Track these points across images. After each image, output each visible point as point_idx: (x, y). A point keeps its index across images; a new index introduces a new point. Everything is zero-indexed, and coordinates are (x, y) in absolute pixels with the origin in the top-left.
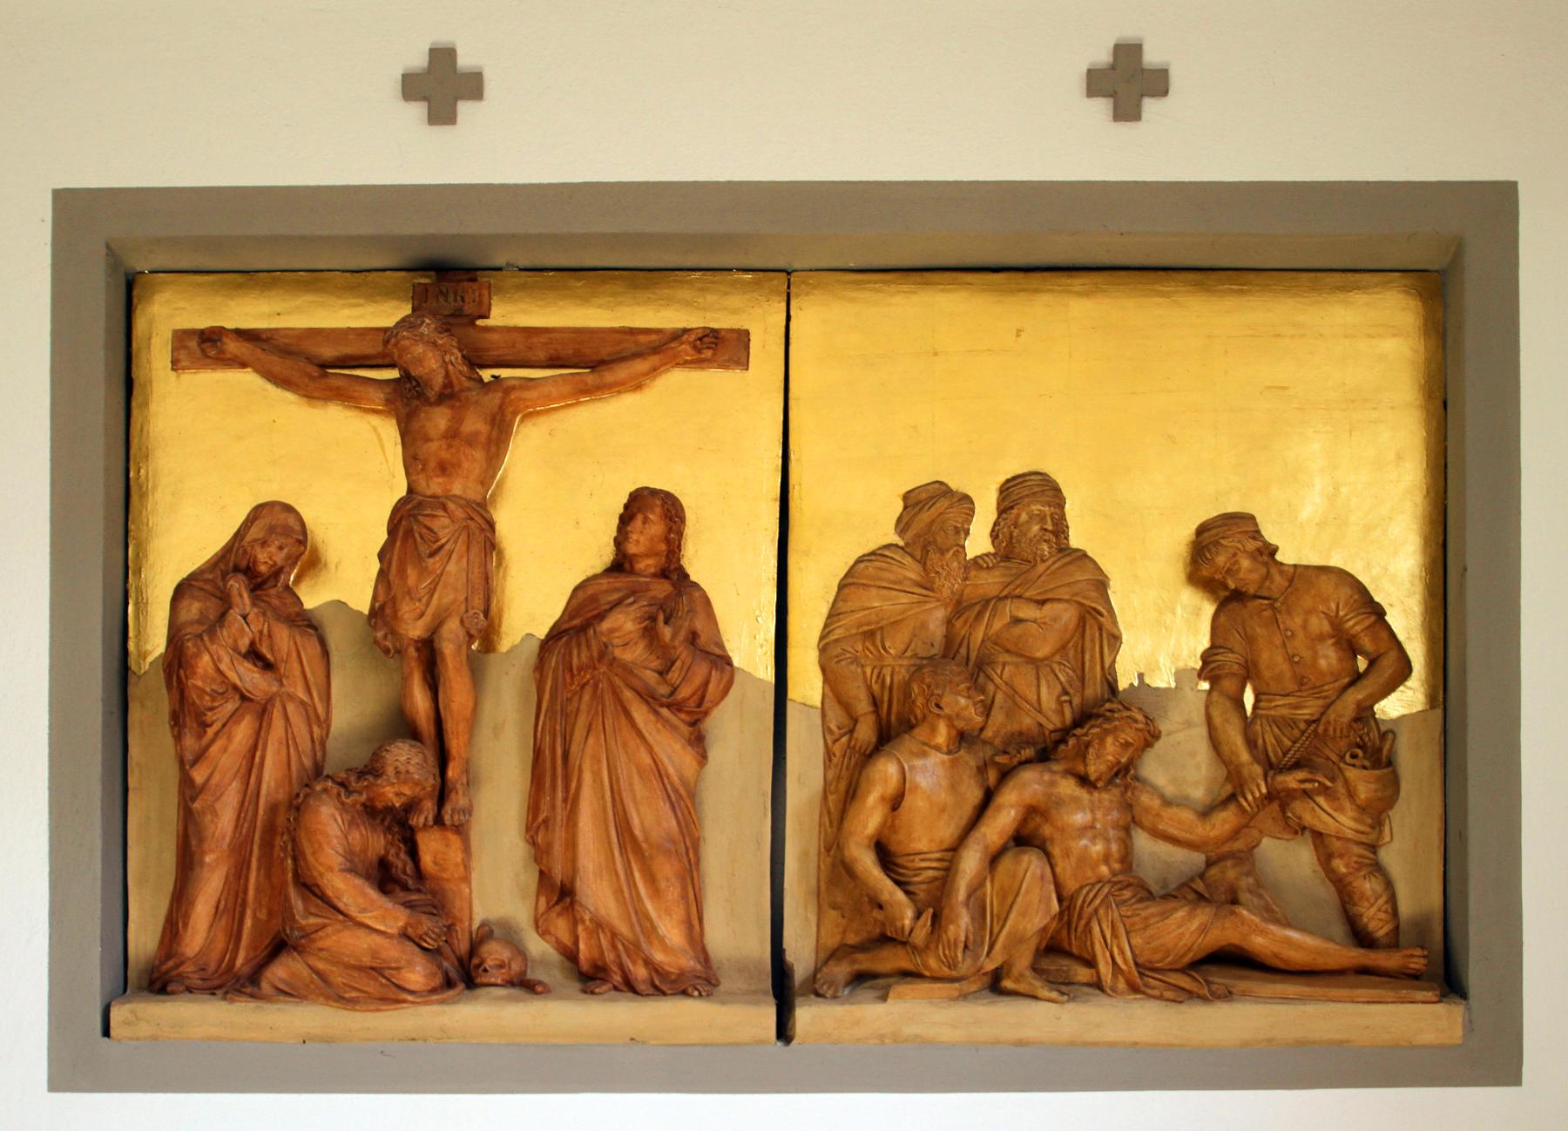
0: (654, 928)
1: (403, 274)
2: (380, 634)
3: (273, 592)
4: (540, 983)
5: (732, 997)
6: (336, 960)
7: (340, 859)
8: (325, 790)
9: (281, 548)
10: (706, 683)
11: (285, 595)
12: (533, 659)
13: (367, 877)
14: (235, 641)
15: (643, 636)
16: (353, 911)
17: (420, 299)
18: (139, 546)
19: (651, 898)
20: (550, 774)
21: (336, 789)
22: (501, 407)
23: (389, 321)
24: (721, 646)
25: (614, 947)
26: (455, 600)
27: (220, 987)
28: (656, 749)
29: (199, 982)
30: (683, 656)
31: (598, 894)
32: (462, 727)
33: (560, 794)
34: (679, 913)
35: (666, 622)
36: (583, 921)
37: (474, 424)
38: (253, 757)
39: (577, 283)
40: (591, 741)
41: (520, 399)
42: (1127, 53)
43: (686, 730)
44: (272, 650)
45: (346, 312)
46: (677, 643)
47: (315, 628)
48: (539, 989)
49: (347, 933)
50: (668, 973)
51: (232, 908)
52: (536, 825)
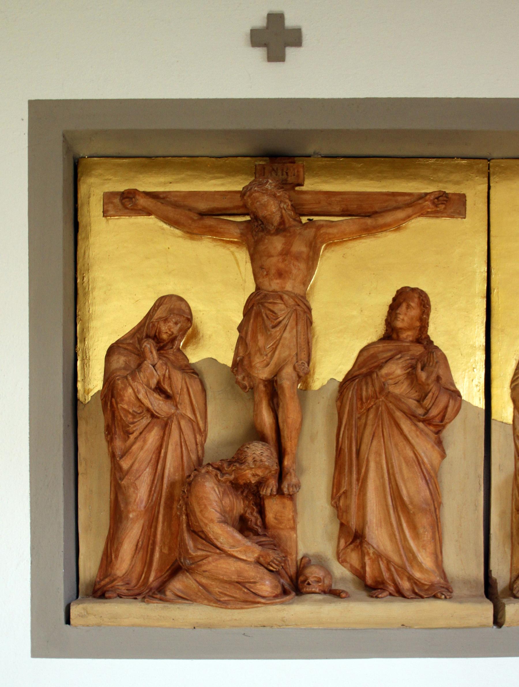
0: (415, 557)
1: (248, 159)
2: (240, 377)
3: (171, 351)
4: (343, 591)
5: (461, 600)
6: (215, 578)
7: (218, 515)
8: (208, 472)
9: (176, 323)
10: (446, 408)
11: (178, 354)
12: (336, 394)
13: (233, 526)
14: (148, 380)
15: (407, 378)
16: (226, 548)
17: (260, 173)
18: (83, 324)
19: (413, 539)
20: (347, 463)
21: (214, 472)
22: (315, 237)
23: (240, 188)
24: (453, 384)
25: (389, 570)
26: (290, 355)
27: (139, 594)
28: (417, 448)
29: (126, 591)
30: (433, 390)
31: (379, 537)
32: (294, 434)
33: (355, 476)
34: (430, 548)
35: (422, 369)
36: (368, 554)
37: (299, 247)
38: (160, 453)
39: (358, 165)
40: (375, 443)
41: (326, 233)
42: (275, 19)
43: (433, 436)
44: (171, 386)
45: (213, 182)
46: (430, 381)
47: (197, 375)
48: (343, 595)
49: (222, 561)
50: (424, 585)
51: (146, 546)
52: (338, 495)
